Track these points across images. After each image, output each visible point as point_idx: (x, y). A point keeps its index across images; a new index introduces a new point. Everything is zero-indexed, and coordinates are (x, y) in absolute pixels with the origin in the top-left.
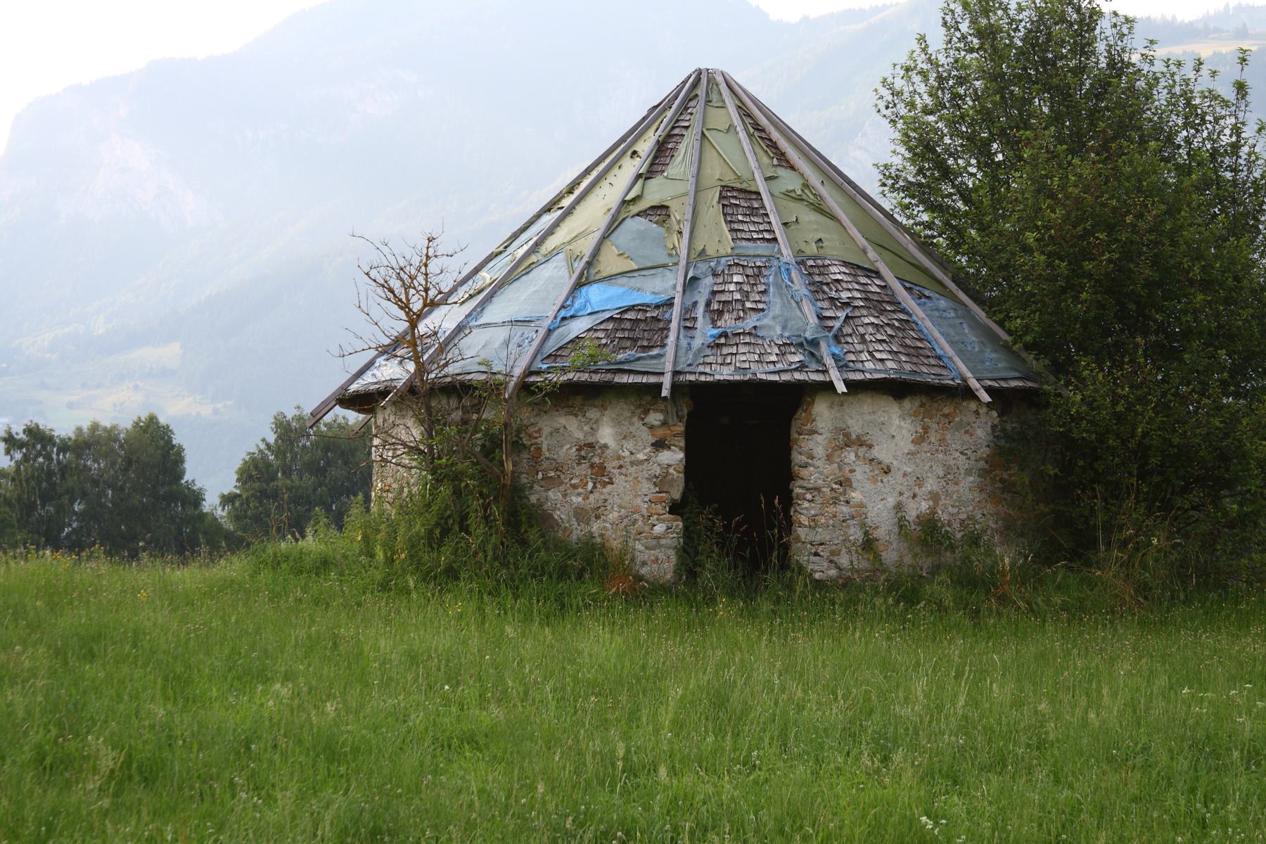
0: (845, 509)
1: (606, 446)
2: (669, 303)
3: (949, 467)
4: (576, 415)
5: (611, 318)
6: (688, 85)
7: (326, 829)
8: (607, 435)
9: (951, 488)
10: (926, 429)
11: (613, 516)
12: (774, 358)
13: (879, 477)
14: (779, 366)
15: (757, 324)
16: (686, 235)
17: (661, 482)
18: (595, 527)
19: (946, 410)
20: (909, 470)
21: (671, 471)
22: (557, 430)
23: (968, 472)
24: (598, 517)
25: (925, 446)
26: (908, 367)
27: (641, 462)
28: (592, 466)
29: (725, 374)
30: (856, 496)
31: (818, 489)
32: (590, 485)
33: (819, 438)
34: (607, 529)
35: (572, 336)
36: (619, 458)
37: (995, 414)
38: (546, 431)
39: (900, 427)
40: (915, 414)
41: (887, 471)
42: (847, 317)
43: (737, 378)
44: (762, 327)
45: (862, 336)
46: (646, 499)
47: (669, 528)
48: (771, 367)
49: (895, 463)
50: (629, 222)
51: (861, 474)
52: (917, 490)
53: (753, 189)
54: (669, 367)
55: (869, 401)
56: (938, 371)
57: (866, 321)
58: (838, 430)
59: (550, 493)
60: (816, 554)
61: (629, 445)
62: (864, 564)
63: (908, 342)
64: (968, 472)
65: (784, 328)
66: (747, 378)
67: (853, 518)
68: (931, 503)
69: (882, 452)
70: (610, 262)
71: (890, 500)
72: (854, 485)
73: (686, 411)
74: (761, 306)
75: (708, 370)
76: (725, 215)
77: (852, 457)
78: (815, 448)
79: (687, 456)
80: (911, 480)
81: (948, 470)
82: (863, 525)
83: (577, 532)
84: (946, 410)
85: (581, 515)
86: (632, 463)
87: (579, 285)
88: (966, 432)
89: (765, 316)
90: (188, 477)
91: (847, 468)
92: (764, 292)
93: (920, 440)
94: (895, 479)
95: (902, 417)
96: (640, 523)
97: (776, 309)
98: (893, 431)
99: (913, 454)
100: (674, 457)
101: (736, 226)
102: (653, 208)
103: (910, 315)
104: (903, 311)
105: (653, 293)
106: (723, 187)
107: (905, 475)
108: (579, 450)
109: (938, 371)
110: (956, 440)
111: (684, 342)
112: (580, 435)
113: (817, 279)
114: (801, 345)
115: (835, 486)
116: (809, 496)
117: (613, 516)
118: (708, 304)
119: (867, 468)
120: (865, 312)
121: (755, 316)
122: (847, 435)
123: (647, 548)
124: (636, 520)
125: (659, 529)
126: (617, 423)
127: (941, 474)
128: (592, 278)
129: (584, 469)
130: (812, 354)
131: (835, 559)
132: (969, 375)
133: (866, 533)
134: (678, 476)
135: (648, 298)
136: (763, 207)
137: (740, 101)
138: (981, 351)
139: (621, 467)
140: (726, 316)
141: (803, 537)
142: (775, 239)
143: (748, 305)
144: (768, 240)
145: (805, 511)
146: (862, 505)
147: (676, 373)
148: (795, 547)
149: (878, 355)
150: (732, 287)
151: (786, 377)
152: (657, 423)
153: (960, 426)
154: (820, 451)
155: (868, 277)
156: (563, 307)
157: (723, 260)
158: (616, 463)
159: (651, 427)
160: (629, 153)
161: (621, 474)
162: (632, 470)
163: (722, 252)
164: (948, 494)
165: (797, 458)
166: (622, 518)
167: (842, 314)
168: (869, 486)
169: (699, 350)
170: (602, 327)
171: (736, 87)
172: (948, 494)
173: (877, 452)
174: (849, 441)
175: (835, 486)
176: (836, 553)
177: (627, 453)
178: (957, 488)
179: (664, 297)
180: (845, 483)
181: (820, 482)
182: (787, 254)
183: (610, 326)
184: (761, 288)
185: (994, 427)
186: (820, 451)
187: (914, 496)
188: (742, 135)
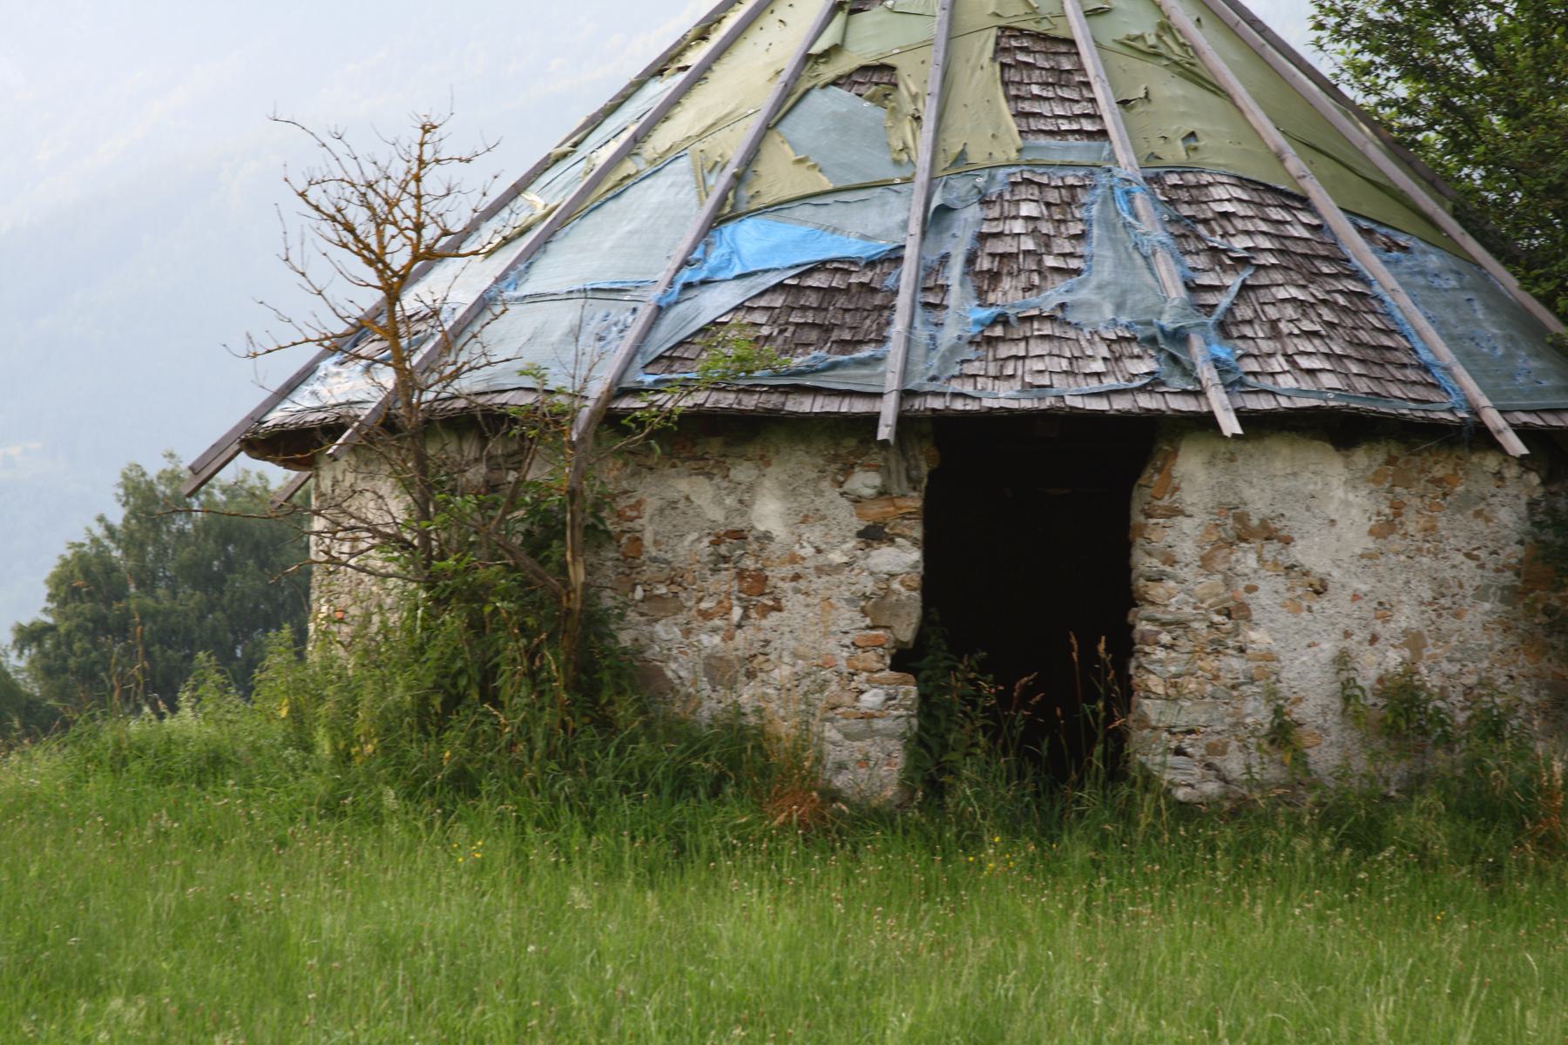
0: (1237, 664)
1: (767, 537)
2: (894, 258)
4: (710, 476)
5: (780, 286)
9: (1447, 624)
10: (1398, 508)
11: (782, 673)
12: (1098, 366)
14: (1109, 383)
15: (1067, 299)
17: (875, 606)
18: (747, 694)
19: (1438, 471)
20: (1364, 588)
21: (896, 585)
22: (673, 504)
23: (1481, 593)
24: (751, 675)
25: (1396, 541)
26: (1363, 386)
27: (838, 568)
28: (741, 575)
29: (1002, 396)
30: (1258, 638)
31: (1183, 624)
32: (737, 613)
33: (1186, 524)
34: (768, 698)
36: (793, 559)
37: (1534, 479)
39: (1347, 504)
40: (1377, 479)
41: (1320, 590)
42: (1245, 287)
43: (1027, 404)
44: (1076, 306)
45: (1274, 323)
46: (847, 641)
48: (1094, 385)
49: (1336, 573)
50: (816, 95)
51: (1268, 595)
52: (1378, 627)
53: (1061, 33)
54: (892, 383)
55: (1285, 451)
56: (1422, 393)
57: (1282, 294)
58: (1225, 508)
59: (659, 628)
60: (1179, 752)
61: (814, 534)
63: (1364, 336)
64: (1481, 593)
65: (1119, 307)
67: (1252, 680)
68: (1407, 653)
69: (1311, 553)
70: (780, 175)
72: (1255, 616)
73: (925, 469)
74: (1074, 264)
75: (968, 388)
76: (1005, 84)
77: (1251, 561)
80: (1368, 607)
83: (710, 704)
84: (1438, 471)
85: (718, 670)
86: (820, 570)
87: (719, 219)
88: (1478, 514)
89: (1082, 284)
91: (1241, 584)
92: (1080, 237)
93: (1385, 529)
94: (1335, 606)
95: (1352, 485)
96: (834, 687)
98: (1332, 510)
100: (901, 559)
101: (1027, 106)
102: (864, 69)
105: (864, 237)
106: (1003, 29)
107: (1356, 597)
108: (716, 543)
109: (1422, 393)
110: (1457, 530)
111: (922, 334)
112: (716, 514)
113: (1186, 211)
114: (1152, 341)
115: (1217, 618)
116: (1165, 638)
118: (971, 259)
119: (1281, 583)
120: (1278, 277)
122: (1242, 518)
123: (847, 736)
125: (872, 699)
126: (790, 491)
127: (1427, 596)
129: (724, 581)
131: (1217, 760)
133: (1278, 711)
134: (909, 597)
135: (853, 248)
136: (1081, 69)
138: (1508, 356)
139: (796, 577)
140: (1006, 283)
141: (1153, 717)
142: (1103, 133)
143: (1050, 261)
144: (1090, 135)
145: (1158, 667)
146: (1269, 657)
148: (1138, 736)
149: (1304, 363)
150: (1018, 227)
151: (1121, 404)
152: (868, 492)
153: (1466, 501)
154: (1187, 550)
158: (787, 570)
159: (857, 500)
161: (797, 591)
162: (819, 583)
163: (1000, 157)
164: (1440, 636)
165: (1144, 562)
166: (798, 678)
167: (1233, 281)
168: (1284, 618)
169: (953, 350)
170: (763, 303)
172: (1440, 636)
173: (1299, 553)
174: (1243, 529)
175: (1217, 618)
177: (808, 551)
178: (1457, 624)
179: (885, 245)
180: (1237, 612)
181: (1188, 610)
183: (778, 301)
184: (1076, 228)
186: (1187, 550)
187: (1374, 639)
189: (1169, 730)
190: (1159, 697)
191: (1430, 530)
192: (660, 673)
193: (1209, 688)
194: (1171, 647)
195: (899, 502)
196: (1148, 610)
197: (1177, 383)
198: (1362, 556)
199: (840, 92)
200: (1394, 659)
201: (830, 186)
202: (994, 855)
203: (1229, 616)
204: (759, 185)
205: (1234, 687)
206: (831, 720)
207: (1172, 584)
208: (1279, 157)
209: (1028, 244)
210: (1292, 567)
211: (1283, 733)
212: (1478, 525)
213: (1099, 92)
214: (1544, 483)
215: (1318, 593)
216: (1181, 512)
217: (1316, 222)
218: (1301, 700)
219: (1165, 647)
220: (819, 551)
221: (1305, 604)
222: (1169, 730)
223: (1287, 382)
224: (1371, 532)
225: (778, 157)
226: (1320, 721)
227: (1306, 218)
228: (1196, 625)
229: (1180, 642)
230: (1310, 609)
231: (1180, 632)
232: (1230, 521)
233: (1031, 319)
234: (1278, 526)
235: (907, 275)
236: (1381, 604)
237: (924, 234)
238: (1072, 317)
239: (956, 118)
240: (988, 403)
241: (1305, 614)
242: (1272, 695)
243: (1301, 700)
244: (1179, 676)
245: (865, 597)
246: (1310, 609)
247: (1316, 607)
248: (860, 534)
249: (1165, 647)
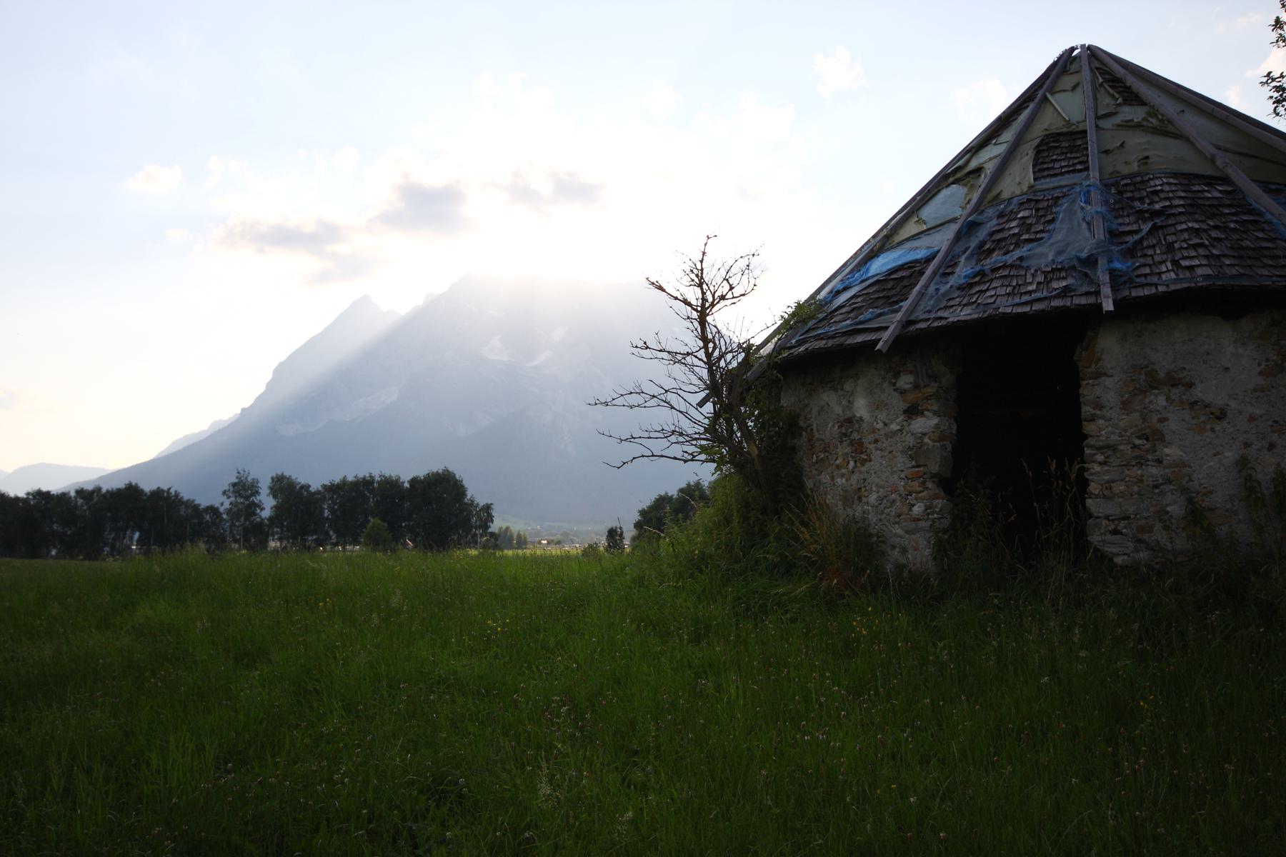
0: (1154, 470)
1: (861, 419)
4: (836, 390)
5: (877, 282)
6: (1057, 68)
8: (861, 407)
17: (916, 453)
18: (858, 511)
20: (1258, 412)
21: (926, 440)
27: (895, 433)
28: (851, 444)
30: (1172, 452)
31: (1113, 448)
33: (1108, 382)
36: (874, 431)
41: (1221, 415)
44: (1028, 257)
46: (903, 475)
47: (927, 508)
48: (1026, 298)
49: (1232, 404)
52: (1275, 437)
60: (1116, 532)
61: (882, 416)
67: (1169, 482)
69: (1210, 391)
71: (1228, 454)
72: (1168, 438)
77: (1162, 401)
82: (1184, 491)
86: (887, 436)
90: (469, 494)
91: (1155, 418)
96: (898, 503)
103: (1261, 214)
107: (1251, 419)
112: (838, 410)
115: (1138, 442)
116: (1100, 458)
117: (873, 498)
123: (907, 532)
124: (894, 502)
130: (1086, 275)
131: (1145, 537)
133: (1190, 501)
139: (876, 441)
145: (1098, 473)
146: (1181, 464)
152: (908, 386)
154: (1111, 398)
158: (871, 438)
159: (903, 392)
161: (877, 449)
166: (881, 499)
167: (1146, 227)
173: (1198, 392)
175: (1138, 442)
177: (881, 425)
180: (1155, 437)
181: (1114, 438)
189: (1107, 518)
190: (1097, 496)
193: (1136, 488)
194: (1105, 463)
195: (924, 390)
196: (1089, 441)
198: (1255, 390)
203: (1147, 440)
205: (1156, 487)
206: (897, 523)
207: (1101, 422)
208: (1212, 160)
210: (1196, 402)
211: (1196, 515)
215: (1219, 418)
216: (1105, 375)
217: (1229, 189)
218: (1211, 492)
219: (1100, 464)
220: (885, 424)
221: (1208, 427)
222: (1107, 518)
224: (1261, 373)
226: (1229, 506)
228: (1122, 447)
229: (1111, 460)
230: (1212, 430)
231: (1110, 453)
232: (1143, 376)
233: (999, 268)
234: (1181, 375)
236: (1276, 422)
238: (1024, 264)
241: (1208, 434)
242: (1184, 491)
243: (1211, 492)
244: (1113, 481)
245: (910, 448)
246: (1212, 430)
247: (1217, 428)
248: (905, 412)
249: (1100, 464)
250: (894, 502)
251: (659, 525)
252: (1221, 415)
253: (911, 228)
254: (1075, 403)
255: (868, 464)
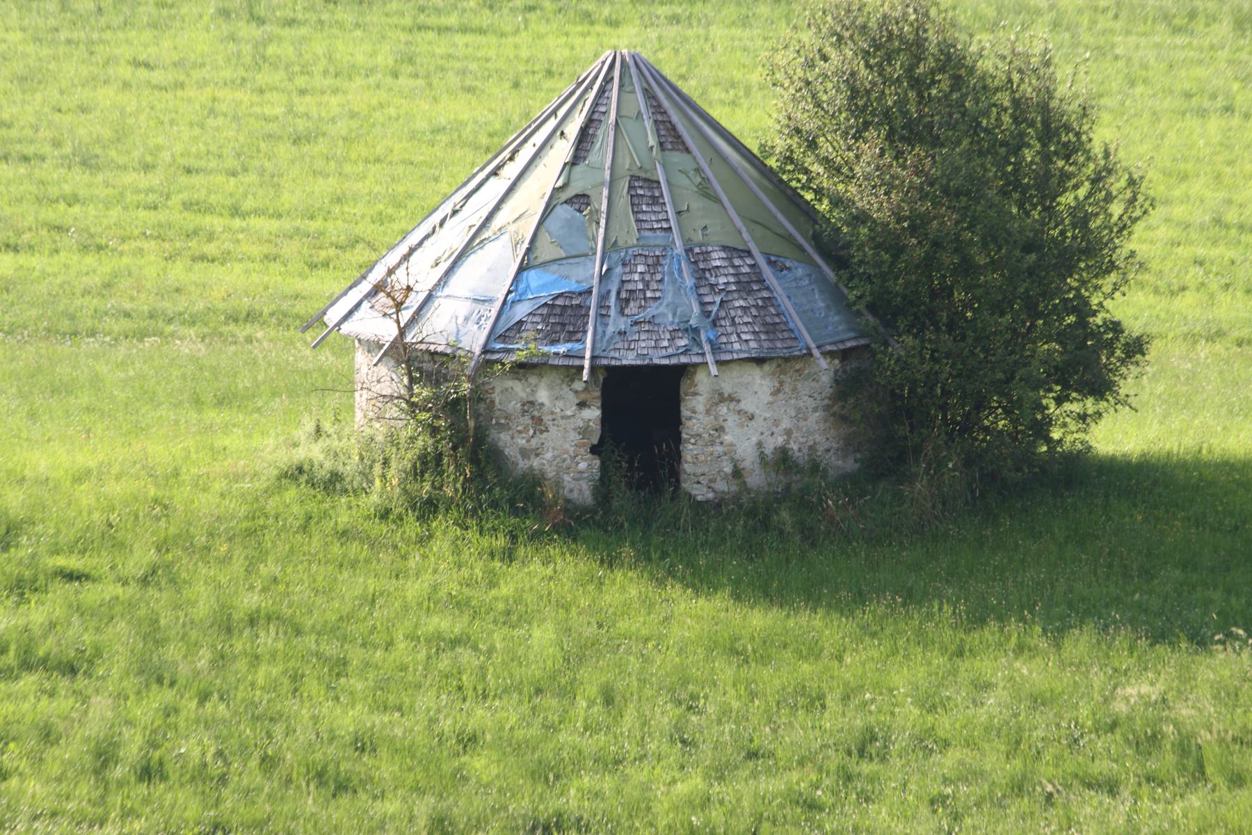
1: (542, 404)
2: (589, 292)
3: (800, 409)
4: (520, 380)
5: (546, 304)
7: (422, 821)
8: (543, 396)
9: (802, 423)
10: (781, 383)
11: (549, 455)
12: (665, 343)
13: (746, 422)
14: (670, 351)
15: (655, 313)
16: (603, 222)
17: (584, 431)
18: (536, 463)
22: (507, 390)
23: (815, 410)
24: (537, 455)
25: (781, 396)
26: (766, 345)
27: (569, 417)
28: (533, 418)
29: (629, 359)
30: (728, 438)
31: (699, 435)
32: (531, 432)
33: (700, 398)
34: (546, 462)
35: (517, 319)
36: (552, 413)
37: (837, 361)
38: (498, 390)
39: (761, 385)
40: (773, 374)
41: (752, 418)
42: (722, 301)
43: (639, 362)
44: (658, 315)
45: (733, 319)
48: (664, 352)
50: (558, 207)
51: (731, 422)
52: (774, 429)
53: (655, 178)
54: (588, 355)
56: (790, 343)
57: (737, 304)
58: (714, 391)
59: (502, 436)
60: (699, 483)
61: (560, 404)
62: (734, 488)
63: (768, 319)
64: (815, 410)
65: (674, 315)
66: (646, 362)
67: (725, 454)
69: (747, 405)
70: (547, 250)
73: (601, 378)
74: (658, 294)
75: (617, 355)
76: (633, 205)
77: (725, 410)
78: (696, 410)
79: (603, 413)
81: (799, 410)
82: (732, 459)
83: (523, 465)
84: (798, 367)
85: (525, 453)
86: (562, 417)
87: (521, 269)
89: (661, 304)
92: (661, 281)
93: (776, 392)
94: (758, 424)
95: (763, 377)
97: (669, 298)
99: (771, 403)
100: (593, 414)
101: (641, 216)
102: (577, 196)
104: (768, 288)
105: (578, 282)
106: (632, 176)
108: (523, 405)
109: (790, 343)
110: (805, 387)
111: (600, 329)
112: (523, 395)
113: (702, 266)
114: (687, 330)
117: (549, 455)
118: (618, 293)
119: (736, 417)
120: (736, 295)
121: (654, 305)
122: (721, 394)
124: (564, 460)
125: (583, 466)
126: (550, 388)
127: (793, 414)
128: (532, 263)
129: (527, 420)
132: (813, 345)
133: (735, 466)
134: (596, 428)
135: (574, 287)
136: (662, 196)
137: (647, 82)
138: (826, 316)
140: (632, 304)
141: (688, 471)
142: (670, 228)
143: (649, 294)
144: (665, 229)
145: (690, 451)
146: (732, 445)
147: (593, 358)
148: (683, 477)
149: (744, 337)
150: (636, 277)
151: (674, 361)
154: (700, 408)
155: (740, 257)
156: (509, 292)
157: (630, 252)
158: (550, 417)
159: (576, 392)
160: (558, 133)
162: (562, 422)
163: (630, 243)
164: (799, 429)
165: (685, 413)
166: (555, 458)
167: (718, 299)
169: (612, 338)
170: (539, 312)
171: (642, 65)
172: (799, 429)
173: (742, 406)
174: (722, 398)
176: (713, 481)
177: (558, 410)
179: (585, 286)
180: (720, 429)
182: (679, 248)
183: (545, 311)
184: (659, 277)
185: (836, 372)
186: (700, 408)
188: (648, 124)
191: (794, 389)
192: (502, 452)
197: (696, 350)
199: (565, 206)
200: (780, 440)
201: (564, 255)
202: (627, 551)
204: (537, 253)
209: (640, 286)
211: (737, 473)
212: (814, 384)
213: (669, 208)
214: (841, 362)
223: (737, 346)
225: (544, 238)
227: (749, 261)
235: (593, 301)
237: (600, 281)
239: (615, 225)
240: (625, 362)
242: (732, 459)
250: (564, 460)
251: (849, 697)
252: (752, 418)
253: (598, 337)
254: (678, 412)
255: (545, 434)
